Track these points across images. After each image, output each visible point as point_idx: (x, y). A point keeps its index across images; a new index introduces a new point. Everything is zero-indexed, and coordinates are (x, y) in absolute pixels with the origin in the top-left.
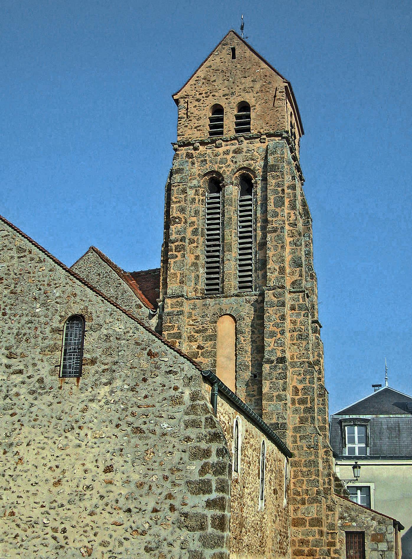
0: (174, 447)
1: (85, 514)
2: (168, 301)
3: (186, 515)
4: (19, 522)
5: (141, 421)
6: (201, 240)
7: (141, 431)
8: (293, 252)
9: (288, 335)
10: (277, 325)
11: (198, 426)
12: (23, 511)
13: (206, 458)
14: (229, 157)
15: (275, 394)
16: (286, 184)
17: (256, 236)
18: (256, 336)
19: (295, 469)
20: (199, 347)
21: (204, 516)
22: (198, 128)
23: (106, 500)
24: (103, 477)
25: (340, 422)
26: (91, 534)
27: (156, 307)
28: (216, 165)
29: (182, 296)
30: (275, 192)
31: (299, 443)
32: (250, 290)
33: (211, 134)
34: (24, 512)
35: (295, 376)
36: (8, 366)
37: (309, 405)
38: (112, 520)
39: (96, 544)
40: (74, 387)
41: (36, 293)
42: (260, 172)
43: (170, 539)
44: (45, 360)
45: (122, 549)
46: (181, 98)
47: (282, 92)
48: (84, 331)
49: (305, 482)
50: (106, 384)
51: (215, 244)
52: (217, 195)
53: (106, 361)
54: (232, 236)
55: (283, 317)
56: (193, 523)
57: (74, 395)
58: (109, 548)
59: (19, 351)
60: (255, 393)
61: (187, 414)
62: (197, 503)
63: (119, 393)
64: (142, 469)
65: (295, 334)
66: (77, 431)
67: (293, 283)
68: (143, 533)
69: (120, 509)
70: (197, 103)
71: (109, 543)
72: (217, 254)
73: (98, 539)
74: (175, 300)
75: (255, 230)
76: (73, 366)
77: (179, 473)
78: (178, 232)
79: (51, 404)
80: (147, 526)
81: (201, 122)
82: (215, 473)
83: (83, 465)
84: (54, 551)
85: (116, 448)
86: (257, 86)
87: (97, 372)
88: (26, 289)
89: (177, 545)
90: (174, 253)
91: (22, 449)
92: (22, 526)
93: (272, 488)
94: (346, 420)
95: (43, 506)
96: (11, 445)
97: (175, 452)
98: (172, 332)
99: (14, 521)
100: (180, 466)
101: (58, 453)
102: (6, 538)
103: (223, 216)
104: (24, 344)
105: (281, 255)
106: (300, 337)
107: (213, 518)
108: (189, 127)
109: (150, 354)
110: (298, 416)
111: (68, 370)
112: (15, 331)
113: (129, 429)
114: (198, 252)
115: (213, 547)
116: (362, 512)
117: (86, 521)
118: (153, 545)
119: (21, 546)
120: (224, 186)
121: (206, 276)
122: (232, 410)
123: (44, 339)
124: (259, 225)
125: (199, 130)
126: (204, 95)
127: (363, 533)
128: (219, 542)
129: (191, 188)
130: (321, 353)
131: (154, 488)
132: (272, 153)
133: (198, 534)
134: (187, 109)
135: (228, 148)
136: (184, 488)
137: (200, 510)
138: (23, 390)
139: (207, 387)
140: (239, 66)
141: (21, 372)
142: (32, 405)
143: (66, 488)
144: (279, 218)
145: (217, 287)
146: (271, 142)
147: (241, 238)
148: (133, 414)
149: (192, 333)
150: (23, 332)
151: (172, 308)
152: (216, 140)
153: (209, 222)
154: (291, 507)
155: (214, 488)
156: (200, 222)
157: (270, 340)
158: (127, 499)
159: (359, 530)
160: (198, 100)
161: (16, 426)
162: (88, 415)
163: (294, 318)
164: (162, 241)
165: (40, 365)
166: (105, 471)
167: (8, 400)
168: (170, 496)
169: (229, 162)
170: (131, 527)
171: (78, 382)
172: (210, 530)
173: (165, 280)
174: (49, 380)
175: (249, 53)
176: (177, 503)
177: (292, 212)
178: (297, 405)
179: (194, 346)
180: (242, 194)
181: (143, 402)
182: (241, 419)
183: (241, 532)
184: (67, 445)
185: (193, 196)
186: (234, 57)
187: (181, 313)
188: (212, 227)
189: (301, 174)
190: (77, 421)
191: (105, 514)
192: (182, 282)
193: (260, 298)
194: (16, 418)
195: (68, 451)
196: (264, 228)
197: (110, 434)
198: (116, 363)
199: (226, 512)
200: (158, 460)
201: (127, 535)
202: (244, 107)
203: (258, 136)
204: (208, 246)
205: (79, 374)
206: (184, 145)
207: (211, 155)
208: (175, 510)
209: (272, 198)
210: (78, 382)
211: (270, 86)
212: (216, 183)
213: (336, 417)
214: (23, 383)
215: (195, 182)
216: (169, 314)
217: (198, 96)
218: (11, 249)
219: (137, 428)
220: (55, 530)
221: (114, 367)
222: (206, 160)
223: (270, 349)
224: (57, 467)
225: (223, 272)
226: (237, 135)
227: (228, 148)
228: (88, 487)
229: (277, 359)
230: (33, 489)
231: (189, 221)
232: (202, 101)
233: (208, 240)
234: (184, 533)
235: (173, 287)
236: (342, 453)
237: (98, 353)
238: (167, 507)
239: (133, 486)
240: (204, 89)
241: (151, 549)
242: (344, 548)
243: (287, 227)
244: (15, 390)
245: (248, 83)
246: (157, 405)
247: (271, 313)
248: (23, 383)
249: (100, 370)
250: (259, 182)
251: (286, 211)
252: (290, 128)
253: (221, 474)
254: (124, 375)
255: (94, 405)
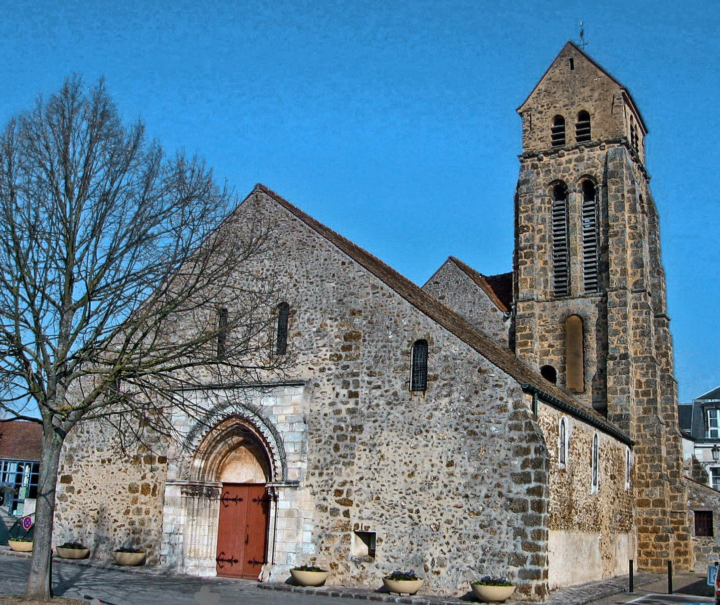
0: (501, 446)
1: (433, 499)
2: (520, 305)
3: (511, 500)
4: (384, 505)
5: (474, 426)
6: (549, 246)
7: (475, 434)
8: (634, 254)
9: (631, 332)
10: (619, 324)
11: (520, 430)
12: (385, 496)
13: (526, 455)
14: (571, 166)
15: (619, 388)
16: (626, 188)
17: (599, 240)
18: (601, 334)
19: (639, 455)
20: (550, 346)
21: (525, 501)
22: (542, 141)
23: (448, 488)
24: (446, 469)
25: (703, 406)
26: (438, 514)
27: (510, 310)
28: (560, 174)
29: (533, 299)
30: (615, 197)
31: (643, 432)
32: (595, 291)
33: (554, 144)
34: (386, 497)
35: (638, 371)
36: (369, 383)
37: (652, 397)
38: (454, 504)
39: (442, 522)
40: (421, 399)
41: (388, 323)
42: (601, 178)
43: (499, 519)
44: (397, 377)
45: (462, 526)
46: (524, 111)
47: (620, 99)
48: (428, 353)
49: (649, 467)
50: (446, 396)
51: (562, 250)
52: (562, 202)
53: (446, 377)
54: (577, 241)
55: (625, 317)
56: (517, 507)
57: (422, 405)
58: (453, 525)
59: (377, 370)
60: (601, 387)
61: (510, 419)
62: (519, 490)
63: (457, 404)
64: (476, 464)
65: (638, 331)
66: (425, 434)
67: (635, 284)
68: (478, 514)
69: (460, 495)
70: (539, 116)
71: (452, 521)
72: (564, 258)
73: (444, 518)
74: (526, 304)
75: (598, 234)
76: (420, 380)
77: (505, 467)
78: (527, 240)
79: (404, 413)
80: (481, 508)
81: (544, 134)
82: (533, 467)
83: (431, 460)
84: (411, 527)
85: (456, 447)
86: (596, 95)
87: (438, 386)
88: (380, 320)
89: (505, 523)
90: (524, 259)
91: (383, 449)
92: (386, 507)
93: (609, 474)
94: (708, 404)
95: (400, 493)
96: (375, 445)
97: (502, 450)
98: (524, 333)
99: (379, 504)
100: (506, 462)
101: (410, 451)
102: (374, 517)
103: (568, 222)
104: (380, 364)
105: (623, 258)
106: (643, 334)
107: (533, 502)
108: (533, 139)
109: (480, 371)
110: (641, 407)
111: (416, 385)
112: (373, 354)
113: (465, 432)
114: (547, 258)
115: (532, 525)
116: (710, 494)
117: (434, 505)
118: (486, 523)
119: (386, 522)
120: (568, 194)
121: (554, 279)
122: (556, 412)
123: (397, 360)
124: (601, 229)
125: (543, 141)
126: (546, 107)
127: (711, 512)
128: (537, 521)
129: (537, 197)
130: (669, 345)
131: (486, 479)
132: (612, 160)
133: (520, 515)
134: (531, 122)
135: (570, 156)
136: (509, 479)
137: (522, 496)
138: (382, 402)
139: (528, 397)
140: (577, 76)
141: (379, 387)
142: (389, 414)
143: (418, 479)
144: (620, 222)
145: (565, 289)
146: (610, 149)
147: (585, 242)
148: (468, 420)
149: (543, 333)
150: (380, 355)
151: (523, 311)
152: (559, 150)
153: (555, 228)
154: (636, 490)
155: (533, 479)
156: (547, 229)
157: (613, 338)
158: (465, 487)
159: (707, 509)
160: (541, 113)
161: (378, 430)
162: (432, 420)
163: (636, 317)
164: (513, 248)
165: (394, 381)
166: (448, 466)
167: (371, 410)
168: (498, 485)
169: (572, 170)
170: (469, 509)
171: (424, 394)
172: (530, 512)
173: (516, 285)
174: (401, 393)
175: (586, 63)
176: (504, 491)
177: (633, 215)
178: (641, 397)
179: (546, 344)
180: (586, 200)
181: (476, 410)
182: (567, 418)
183: (570, 513)
184: (417, 445)
185: (539, 205)
186: (572, 68)
187: (532, 315)
188: (558, 233)
189: (646, 172)
190: (424, 426)
191: (448, 499)
192: (532, 287)
193: (604, 299)
194: (377, 424)
195: (418, 450)
196: (606, 232)
197: (451, 436)
198: (453, 379)
199: (543, 498)
200: (488, 456)
201: (466, 515)
202: (584, 115)
203: (599, 144)
204: (555, 251)
205: (424, 389)
206: (530, 157)
207: (554, 164)
208: (502, 496)
209: (612, 203)
210: (424, 394)
211: (608, 93)
212: (560, 190)
213: (697, 401)
214: (382, 396)
215: (540, 191)
216: (521, 317)
217: (540, 109)
218: (367, 287)
219: (471, 431)
220: (411, 511)
221: (452, 382)
222: (550, 170)
223: (613, 346)
224: (411, 462)
225: (570, 275)
226: (578, 144)
227: (570, 156)
228: (435, 478)
229: (620, 356)
230: (392, 480)
231: (536, 229)
232: (544, 114)
233: (555, 246)
234: (510, 515)
235: (524, 291)
236: (705, 436)
237: (439, 372)
238: (496, 494)
239: (469, 477)
240: (545, 101)
241: (485, 526)
242: (693, 526)
243: (628, 230)
244: (375, 402)
245: (586, 91)
246: (487, 412)
247: (614, 312)
248: (382, 396)
249: (441, 384)
250: (600, 188)
251: (627, 215)
252: (629, 131)
253: (538, 467)
254: (460, 388)
255: (437, 414)
